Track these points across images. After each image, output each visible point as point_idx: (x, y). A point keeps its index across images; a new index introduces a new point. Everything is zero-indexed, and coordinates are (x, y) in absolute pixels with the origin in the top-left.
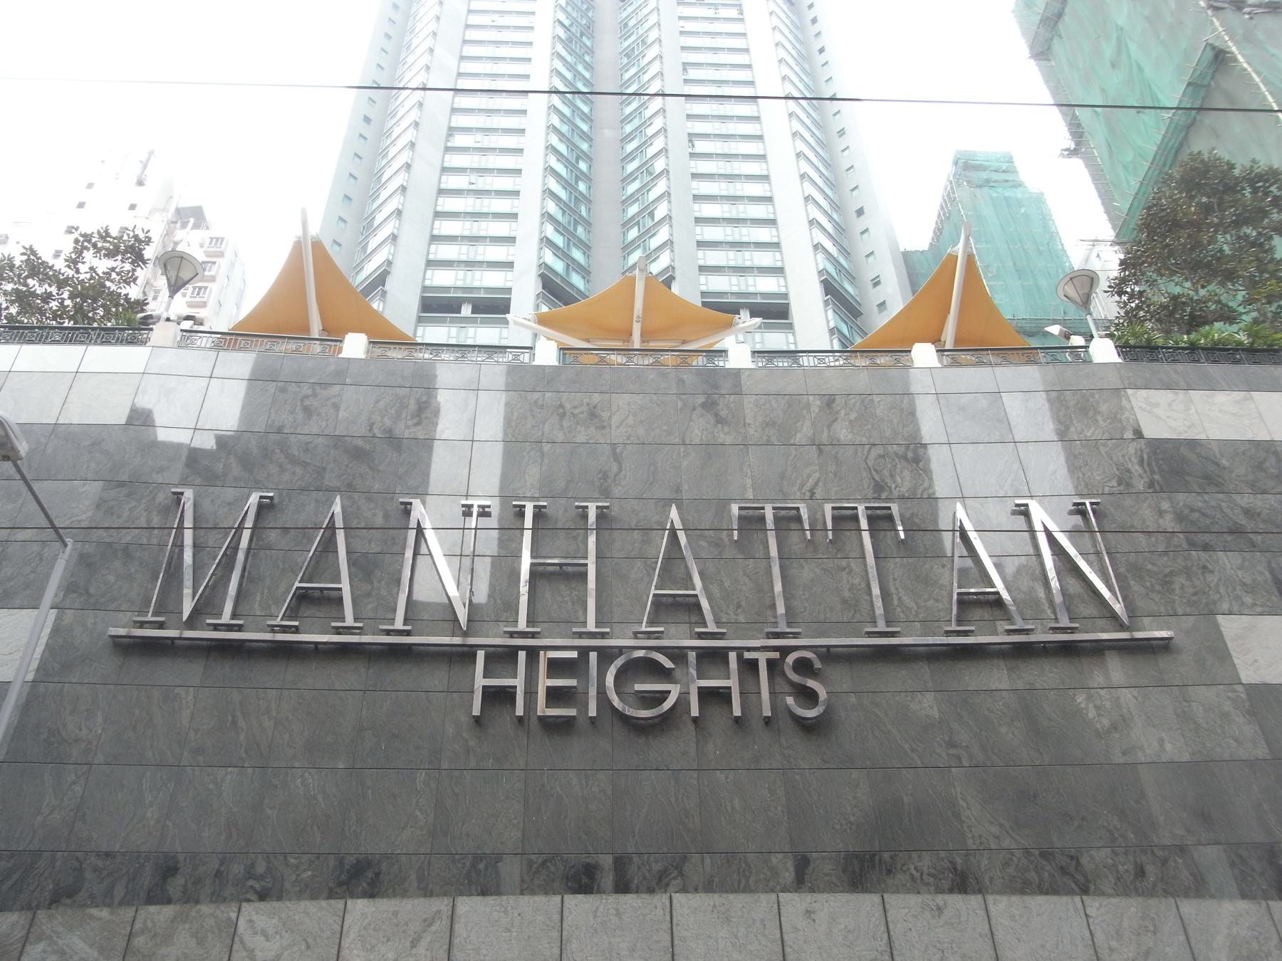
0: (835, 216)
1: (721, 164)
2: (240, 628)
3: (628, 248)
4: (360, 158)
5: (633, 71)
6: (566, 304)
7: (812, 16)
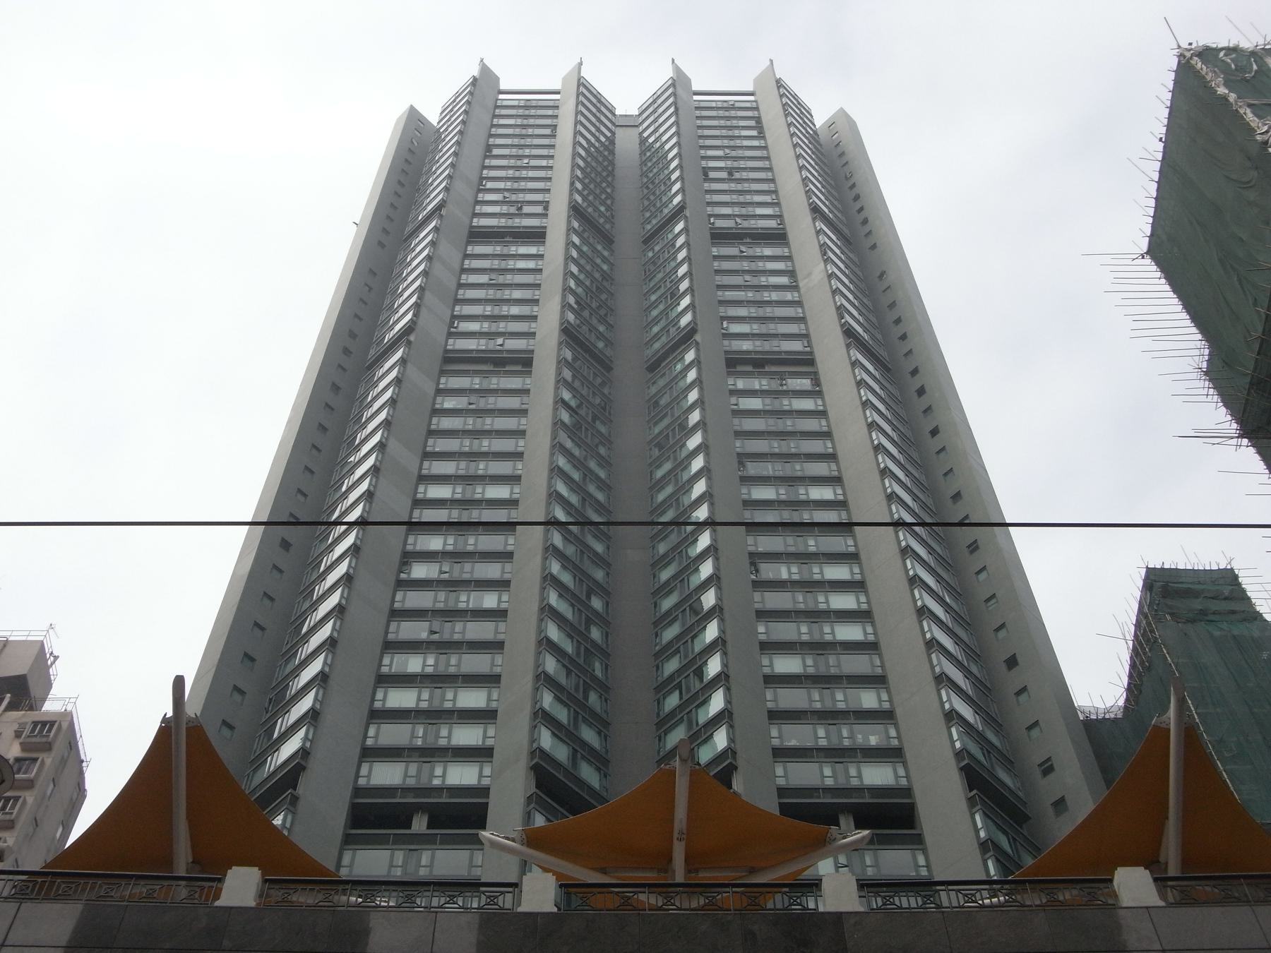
0: (974, 669)
1: (771, 422)
3: (665, 723)
4: (272, 599)
5: (668, 466)
6: (574, 812)
7: (858, 207)
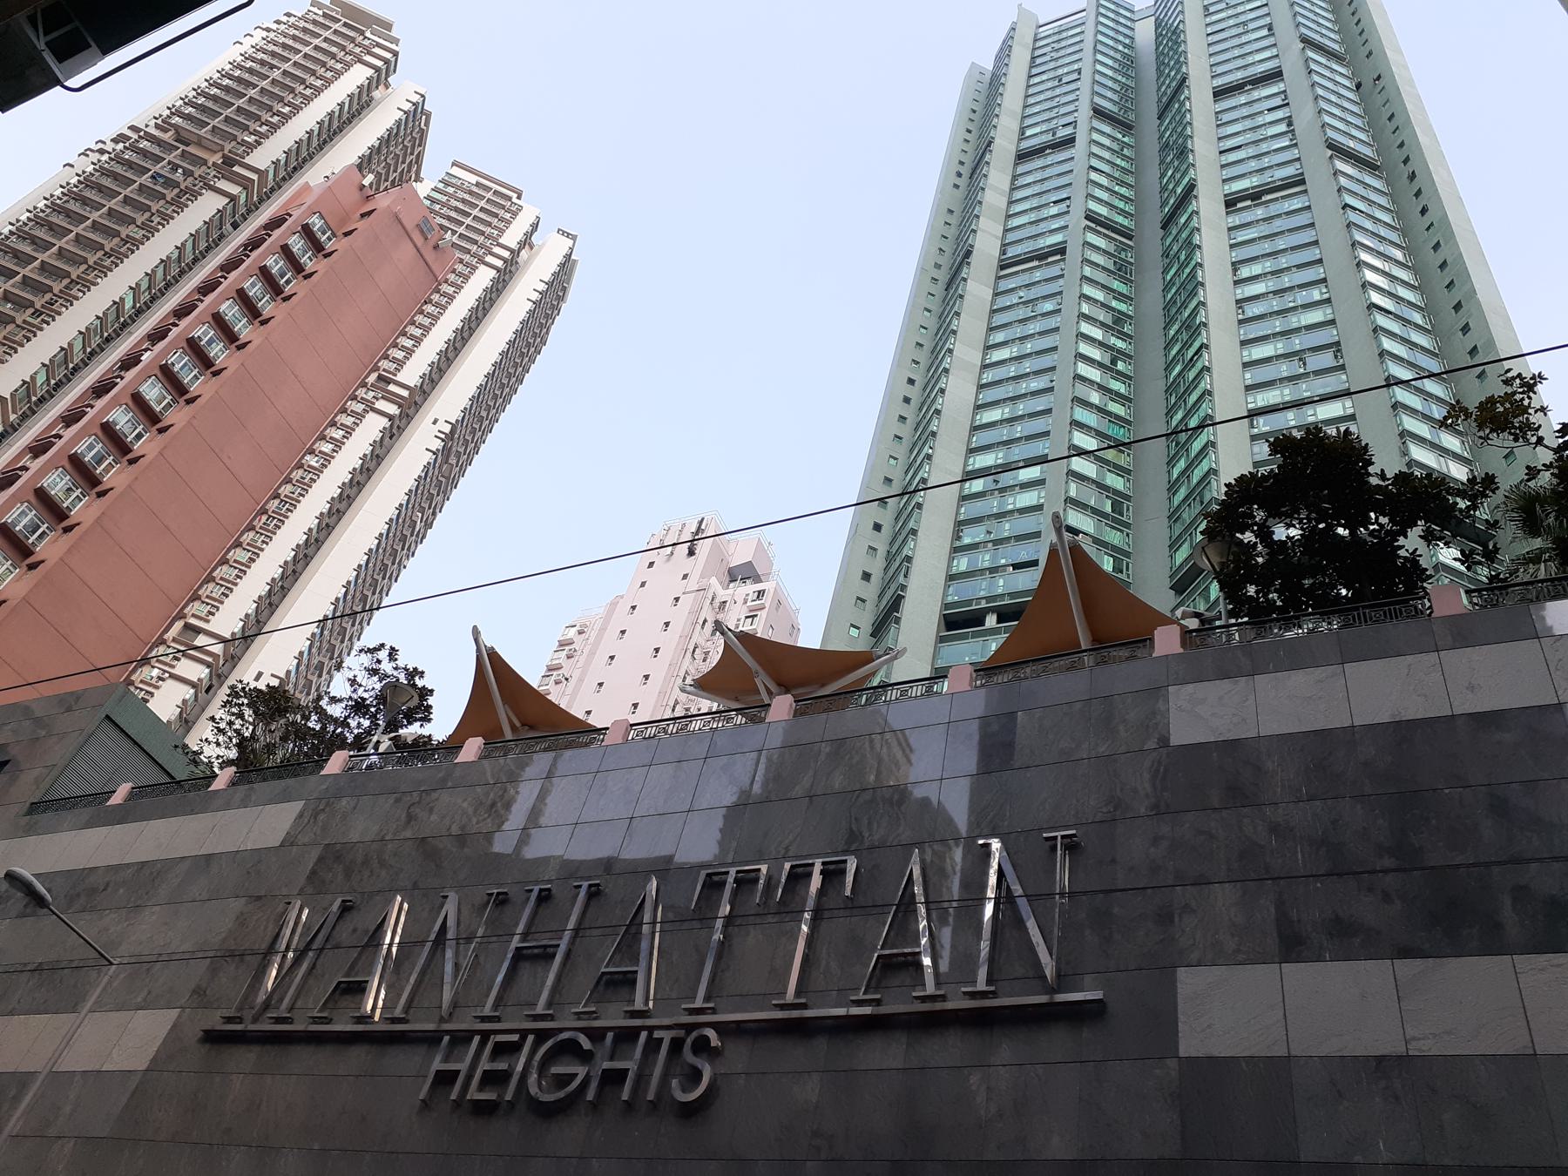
2: (804, 1006)
